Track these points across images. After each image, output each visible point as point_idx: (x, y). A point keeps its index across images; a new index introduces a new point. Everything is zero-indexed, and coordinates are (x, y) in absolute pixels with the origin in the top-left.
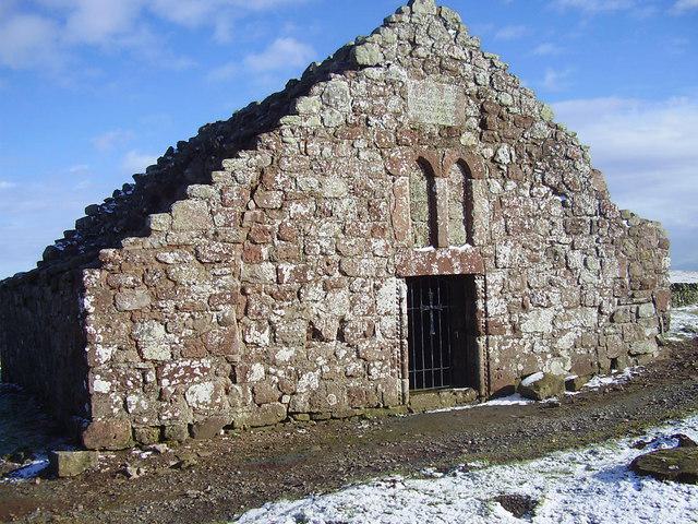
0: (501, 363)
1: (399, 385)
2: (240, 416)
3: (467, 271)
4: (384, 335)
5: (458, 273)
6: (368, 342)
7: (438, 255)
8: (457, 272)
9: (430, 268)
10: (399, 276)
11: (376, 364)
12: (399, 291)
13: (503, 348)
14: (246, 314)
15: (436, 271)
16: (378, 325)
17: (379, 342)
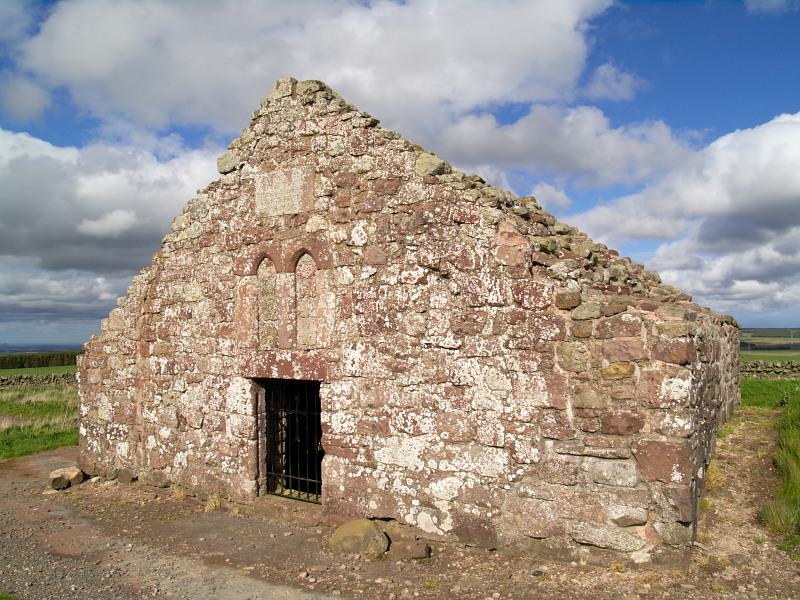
0: (348, 492)
1: (249, 485)
9: (270, 371)
11: (226, 458)
13: (350, 475)
16: (228, 421)
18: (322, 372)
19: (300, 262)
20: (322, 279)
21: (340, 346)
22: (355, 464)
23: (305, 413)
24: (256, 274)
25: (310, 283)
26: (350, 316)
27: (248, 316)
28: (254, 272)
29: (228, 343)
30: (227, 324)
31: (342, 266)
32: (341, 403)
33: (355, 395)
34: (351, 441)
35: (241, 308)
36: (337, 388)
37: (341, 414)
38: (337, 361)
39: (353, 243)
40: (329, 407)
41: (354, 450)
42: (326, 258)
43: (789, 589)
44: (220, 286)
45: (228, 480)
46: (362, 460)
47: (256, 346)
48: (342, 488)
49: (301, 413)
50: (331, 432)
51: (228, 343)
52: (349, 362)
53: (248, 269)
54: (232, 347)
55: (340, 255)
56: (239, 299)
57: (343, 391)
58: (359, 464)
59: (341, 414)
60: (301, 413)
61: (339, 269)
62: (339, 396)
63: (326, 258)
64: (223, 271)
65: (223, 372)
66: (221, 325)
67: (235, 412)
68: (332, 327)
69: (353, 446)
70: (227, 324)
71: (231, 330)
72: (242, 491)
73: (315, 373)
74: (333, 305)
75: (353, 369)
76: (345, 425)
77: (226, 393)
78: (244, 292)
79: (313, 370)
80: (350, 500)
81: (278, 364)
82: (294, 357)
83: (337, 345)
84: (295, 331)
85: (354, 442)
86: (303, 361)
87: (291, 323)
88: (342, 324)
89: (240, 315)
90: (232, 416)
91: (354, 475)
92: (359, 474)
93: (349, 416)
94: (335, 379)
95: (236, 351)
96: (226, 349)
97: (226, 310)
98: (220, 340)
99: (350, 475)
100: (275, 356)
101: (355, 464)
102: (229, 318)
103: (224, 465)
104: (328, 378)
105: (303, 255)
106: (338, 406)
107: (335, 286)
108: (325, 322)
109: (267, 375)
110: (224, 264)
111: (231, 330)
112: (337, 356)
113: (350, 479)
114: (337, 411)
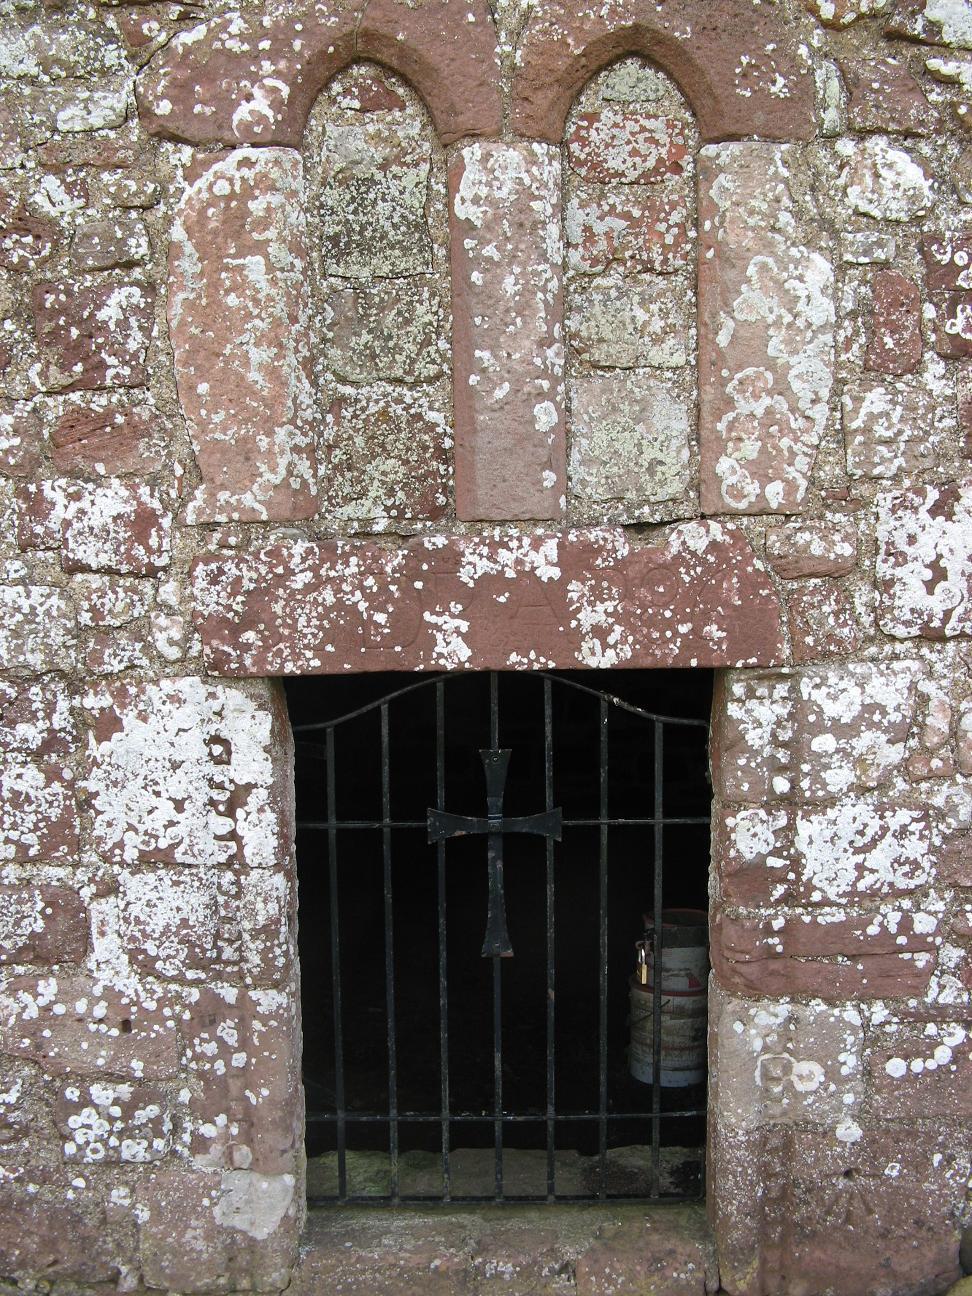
0: (873, 1147)
1: (263, 1201)
2: (340, 544)
3: (670, 653)
4: (144, 966)
5: (606, 660)
6: (49, 988)
7: (474, 566)
8: (598, 657)
9: (423, 638)
10: (217, 671)
11: (100, 1093)
12: (220, 748)
13: (896, 1067)
14: (26, 1006)
15: (453, 647)
16: (103, 910)
17: (111, 995)
18: (753, 629)
19: (587, 103)
20: (748, 184)
21: (863, 503)
22: (920, 1018)
23: (440, 826)
24: (299, 145)
25: (648, 206)
26: (916, 368)
27: (259, 355)
28: (290, 130)
29: (109, 502)
30: (100, 402)
31: (862, 135)
32: (860, 762)
33: (938, 722)
34: (906, 925)
35: (209, 311)
36: (836, 696)
37: (854, 814)
38: (836, 575)
39: (934, 27)
40: (781, 785)
41: (922, 960)
42: (779, 86)
43: (706, 1292)
44: (51, 196)
45: (119, 1196)
46: (947, 998)
47: (301, 512)
48: (850, 1131)
49: (523, 825)
50: (788, 899)
51: (109, 502)
52: (913, 576)
53: (256, 107)
54: (142, 523)
55: (851, 85)
56: (188, 264)
57: (869, 708)
58: (940, 1014)
59: (854, 814)
60: (523, 825)
61: (846, 147)
62: (840, 729)
63: (779, 86)
64: (70, 118)
65: (68, 660)
66: (55, 408)
67: (154, 859)
68: (820, 413)
69: (919, 943)
70: (100, 402)
71: (139, 430)
72: (213, 1232)
73: (713, 631)
74: (821, 311)
75: (936, 604)
76: (879, 858)
77: (87, 766)
78: (231, 227)
79: (706, 618)
80: (893, 1170)
81: (474, 600)
82: (575, 560)
83: (846, 496)
84: (566, 435)
85: (923, 924)
86: (628, 579)
87: (549, 395)
88: (876, 399)
89: (204, 354)
90: (138, 886)
91: (917, 1065)
92: (943, 1055)
93: (903, 816)
94: (833, 654)
95: (166, 543)
96: (104, 534)
97: (92, 328)
98: (54, 490)
99: (896, 1067)
100: (451, 558)
101: (920, 1018)
102: (115, 369)
103: (88, 1128)
104: (785, 650)
105: (620, 58)
106: (839, 777)
107: (827, 225)
108: (782, 388)
109: (399, 657)
110: (74, 77)
111: (139, 430)
112: (846, 550)
113: (893, 1084)
114: (831, 801)
